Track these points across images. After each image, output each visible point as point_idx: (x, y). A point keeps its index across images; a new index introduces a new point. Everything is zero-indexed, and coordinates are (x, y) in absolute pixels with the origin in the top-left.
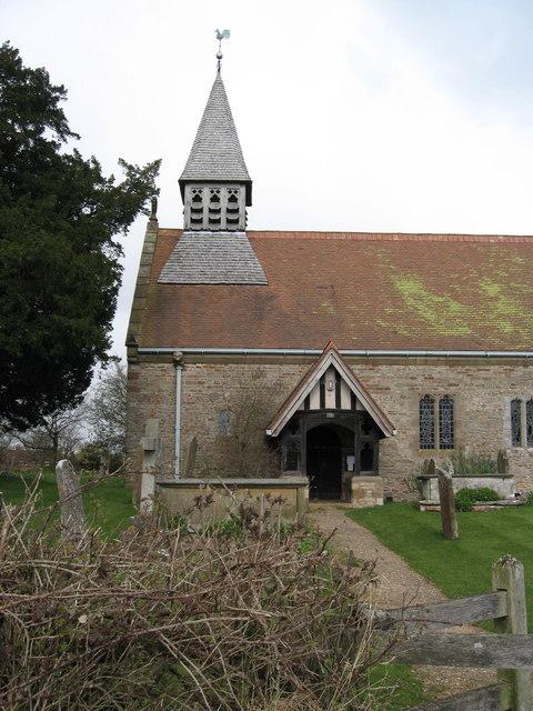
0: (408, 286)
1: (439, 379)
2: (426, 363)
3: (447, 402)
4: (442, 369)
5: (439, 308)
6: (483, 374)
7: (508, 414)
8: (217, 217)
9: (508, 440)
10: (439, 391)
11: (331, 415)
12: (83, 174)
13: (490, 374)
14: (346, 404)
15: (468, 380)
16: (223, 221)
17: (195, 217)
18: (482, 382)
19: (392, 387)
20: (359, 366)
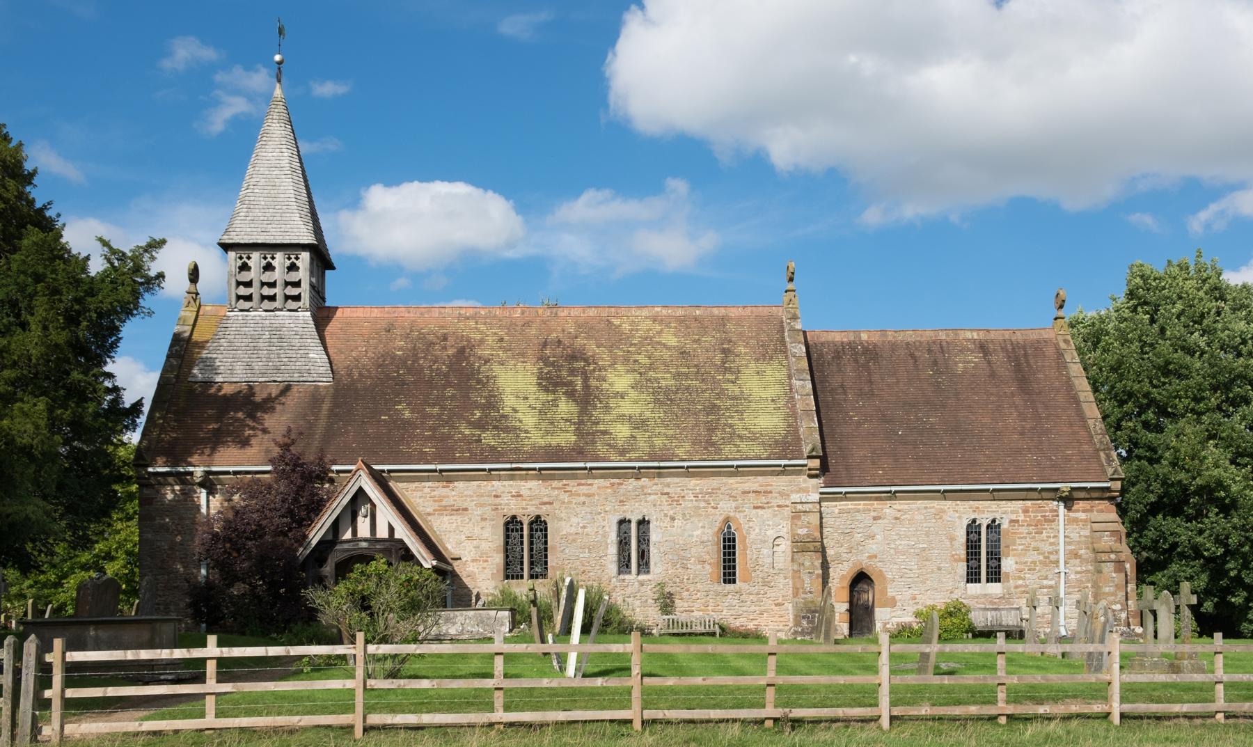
0: (1135, 218)
1: (523, 496)
2: (512, 478)
3: (539, 525)
4: (532, 484)
5: (544, 410)
6: (583, 489)
7: (613, 537)
8: (271, 292)
9: (613, 568)
10: (526, 512)
11: (364, 545)
12: (76, 257)
13: (594, 489)
14: (382, 533)
15: (566, 497)
16: (280, 298)
17: (243, 291)
18: (582, 499)
19: (471, 506)
20: (430, 484)
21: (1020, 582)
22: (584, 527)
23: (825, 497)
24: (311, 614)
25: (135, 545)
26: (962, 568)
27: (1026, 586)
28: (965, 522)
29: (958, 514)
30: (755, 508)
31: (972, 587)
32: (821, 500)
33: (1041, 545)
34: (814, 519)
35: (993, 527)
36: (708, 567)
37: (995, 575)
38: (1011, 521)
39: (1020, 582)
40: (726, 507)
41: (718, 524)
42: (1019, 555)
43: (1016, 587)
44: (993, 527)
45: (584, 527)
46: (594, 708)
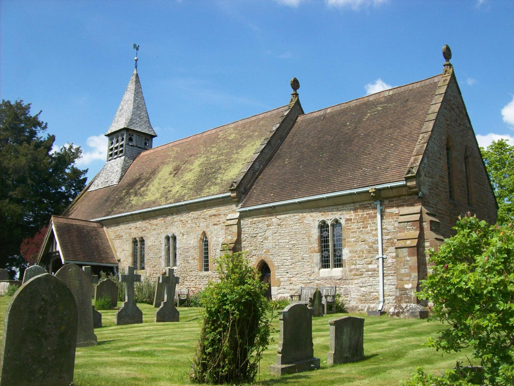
3: (142, 241)
21: (353, 267)
22: (154, 242)
23: (243, 215)
24: (95, 338)
25: (237, 315)
26: (317, 257)
27: (358, 270)
28: (317, 224)
29: (313, 220)
30: (214, 225)
31: (325, 272)
32: (240, 218)
33: (366, 237)
34: (235, 229)
35: (337, 223)
36: (196, 261)
37: (339, 263)
38: (347, 220)
39: (353, 267)
40: (203, 226)
41: (200, 236)
42: (351, 246)
43: (351, 271)
44: (337, 223)
45: (154, 242)
46: (63, 253)
